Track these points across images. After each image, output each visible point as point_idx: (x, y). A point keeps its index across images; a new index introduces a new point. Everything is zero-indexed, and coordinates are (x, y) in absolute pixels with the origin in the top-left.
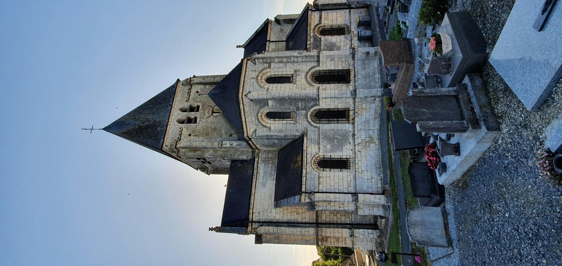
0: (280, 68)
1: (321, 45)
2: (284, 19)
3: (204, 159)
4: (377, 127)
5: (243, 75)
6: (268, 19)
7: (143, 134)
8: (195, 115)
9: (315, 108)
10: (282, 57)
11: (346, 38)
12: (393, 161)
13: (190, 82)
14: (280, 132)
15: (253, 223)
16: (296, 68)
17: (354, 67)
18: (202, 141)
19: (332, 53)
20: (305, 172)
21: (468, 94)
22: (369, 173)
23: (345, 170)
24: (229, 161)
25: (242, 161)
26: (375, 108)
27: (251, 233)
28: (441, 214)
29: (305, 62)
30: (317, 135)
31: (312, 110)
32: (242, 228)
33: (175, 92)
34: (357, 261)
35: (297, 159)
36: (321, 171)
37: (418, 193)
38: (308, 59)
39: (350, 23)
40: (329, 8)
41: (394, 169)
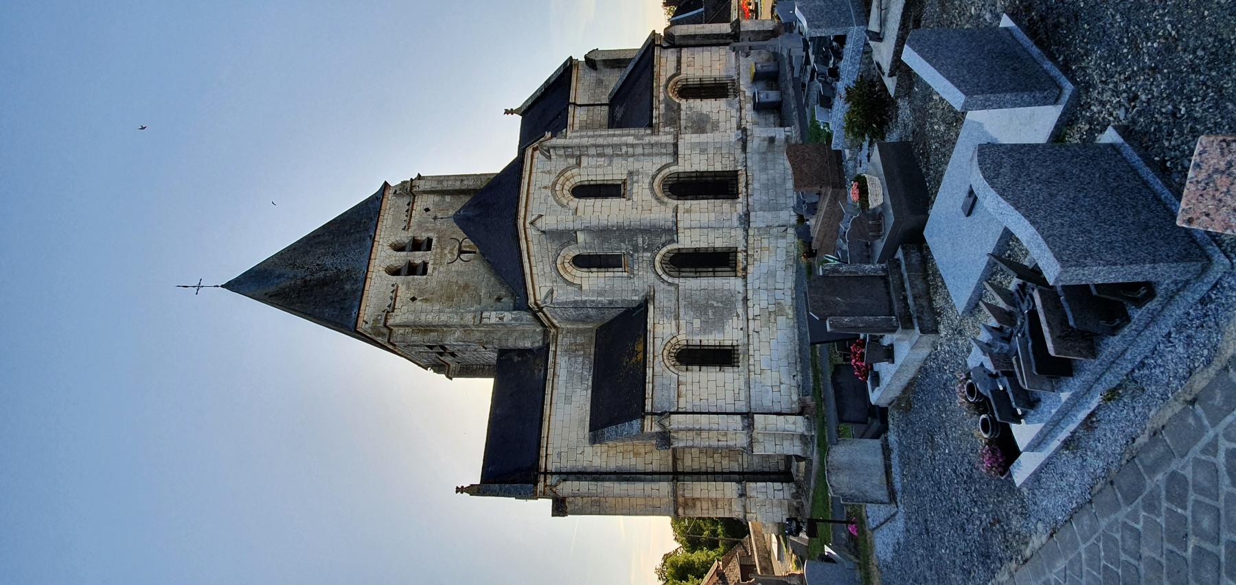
0: (600, 166)
1: (680, 119)
2: (604, 58)
3: (443, 347)
4: (790, 284)
5: (525, 181)
6: (571, 57)
7: (312, 298)
8: (424, 259)
9: (669, 247)
10: (603, 146)
11: (730, 105)
13: (411, 189)
14: (600, 294)
15: (548, 476)
17: (746, 166)
18: (440, 311)
19: (703, 138)
20: (651, 374)
21: (902, 275)
22: (775, 374)
23: (729, 369)
24: (494, 352)
25: (522, 352)
26: (786, 248)
27: (544, 496)
28: (881, 450)
29: (650, 155)
30: (674, 301)
31: (664, 250)
33: (380, 209)
34: (755, 549)
36: (682, 371)
37: (846, 417)
38: (655, 150)
39: (739, 74)
40: (696, 42)
41: (819, 367)
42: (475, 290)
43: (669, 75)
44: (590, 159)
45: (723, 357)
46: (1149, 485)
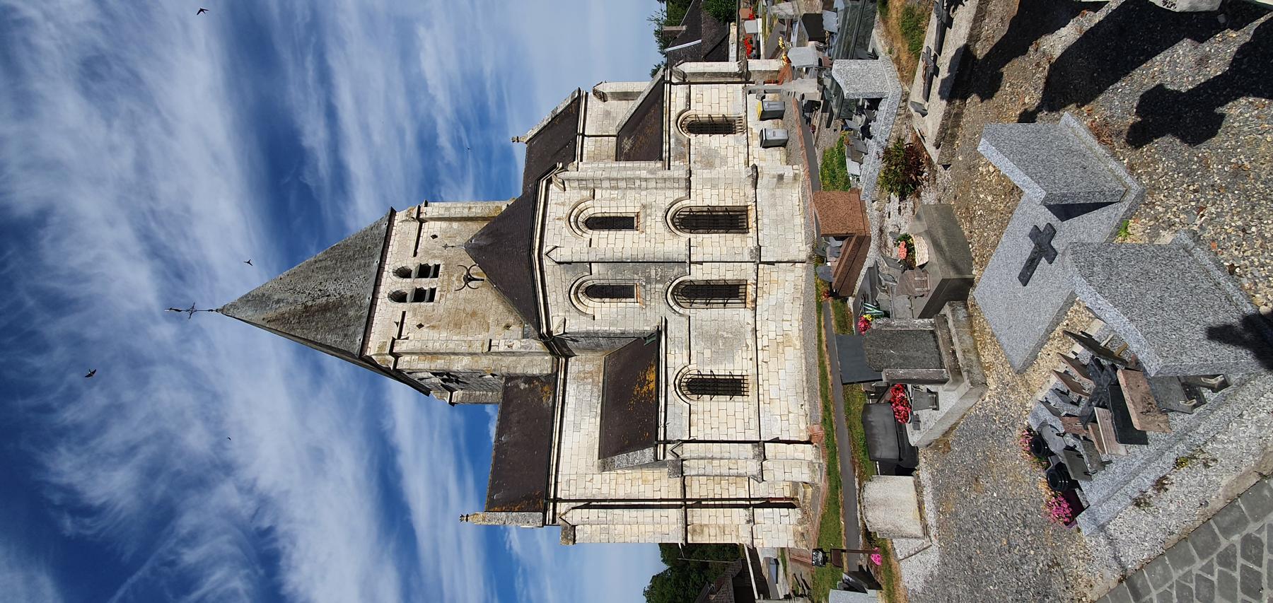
2: (612, 91)
7: (314, 324)
12: (830, 385)
14: (611, 324)
16: (644, 202)
17: (756, 201)
25: (529, 379)
28: (913, 487)
29: (662, 188)
32: (533, 513)
35: (646, 377)
38: (668, 184)
39: (746, 112)
42: (484, 317)
43: (679, 111)
44: (604, 191)
45: (732, 387)
46: (1224, 543)
